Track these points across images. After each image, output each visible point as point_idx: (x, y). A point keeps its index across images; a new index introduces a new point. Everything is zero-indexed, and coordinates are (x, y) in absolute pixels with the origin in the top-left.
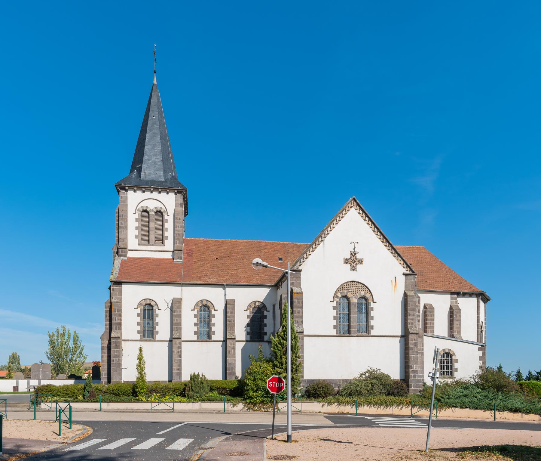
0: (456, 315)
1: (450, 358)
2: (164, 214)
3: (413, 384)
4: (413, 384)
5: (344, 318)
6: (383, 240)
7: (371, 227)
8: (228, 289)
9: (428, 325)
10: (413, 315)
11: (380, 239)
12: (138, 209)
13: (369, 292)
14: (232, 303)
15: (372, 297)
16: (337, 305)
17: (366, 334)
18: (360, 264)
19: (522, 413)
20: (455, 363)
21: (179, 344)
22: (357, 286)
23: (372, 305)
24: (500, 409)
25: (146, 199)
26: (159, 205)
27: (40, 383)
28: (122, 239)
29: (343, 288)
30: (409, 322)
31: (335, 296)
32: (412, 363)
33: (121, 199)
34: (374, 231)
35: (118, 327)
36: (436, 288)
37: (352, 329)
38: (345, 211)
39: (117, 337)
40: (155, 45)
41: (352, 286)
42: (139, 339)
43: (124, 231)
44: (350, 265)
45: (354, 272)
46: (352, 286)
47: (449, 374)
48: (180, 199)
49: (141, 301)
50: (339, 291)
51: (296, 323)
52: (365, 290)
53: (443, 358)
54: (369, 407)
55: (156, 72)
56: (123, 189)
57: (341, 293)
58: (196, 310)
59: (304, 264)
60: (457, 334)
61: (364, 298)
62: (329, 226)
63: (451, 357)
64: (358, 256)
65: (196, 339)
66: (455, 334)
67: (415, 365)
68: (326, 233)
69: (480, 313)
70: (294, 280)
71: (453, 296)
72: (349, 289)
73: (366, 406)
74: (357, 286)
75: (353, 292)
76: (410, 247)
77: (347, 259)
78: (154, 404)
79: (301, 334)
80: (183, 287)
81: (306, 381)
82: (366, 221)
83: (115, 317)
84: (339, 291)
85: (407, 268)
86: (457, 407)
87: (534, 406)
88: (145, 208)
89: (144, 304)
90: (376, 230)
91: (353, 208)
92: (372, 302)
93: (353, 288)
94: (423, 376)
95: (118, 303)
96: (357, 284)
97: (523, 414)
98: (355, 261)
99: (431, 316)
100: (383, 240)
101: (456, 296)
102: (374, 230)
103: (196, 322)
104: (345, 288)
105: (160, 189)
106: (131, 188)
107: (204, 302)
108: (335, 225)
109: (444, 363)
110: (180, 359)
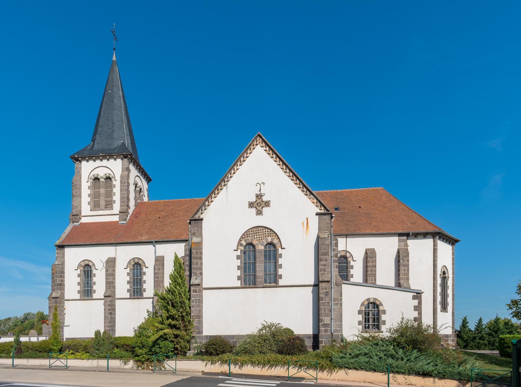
0: (403, 260)
1: (376, 309)
2: (112, 180)
3: (323, 340)
4: (323, 340)
5: (250, 268)
6: (293, 178)
7: (272, 157)
8: (158, 246)
9: (369, 273)
10: (326, 260)
11: (289, 176)
12: (90, 178)
13: (276, 237)
14: (160, 259)
15: (281, 243)
16: (241, 253)
17: (274, 284)
18: (267, 207)
19: (435, 377)
20: (382, 315)
21: (110, 302)
22: (263, 232)
23: (280, 251)
24: (404, 372)
25: (97, 168)
26: (108, 171)
27: (30, 339)
28: (76, 207)
29: (247, 235)
30: (321, 268)
31: (239, 244)
32: (322, 316)
33: (76, 170)
34: (282, 169)
35: (59, 288)
36: (380, 229)
37: (258, 279)
38: (250, 150)
39: (56, 297)
40: (114, 24)
41: (257, 231)
42: (79, 298)
43: (77, 199)
44: (255, 209)
45: (260, 216)
46: (257, 231)
47: (375, 327)
48: (126, 164)
49: (80, 262)
50: (243, 238)
51: (194, 276)
52: (272, 235)
53: (367, 310)
54: (252, 367)
55: (116, 49)
56: (77, 160)
57: (245, 240)
58: (129, 268)
59: (205, 211)
60: (404, 281)
61: (271, 244)
62: (232, 168)
63: (378, 307)
64: (265, 199)
65: (128, 297)
66: (402, 282)
67: (326, 318)
68: (229, 176)
69: (437, 255)
70: (195, 230)
71: (401, 238)
72: (254, 236)
73: (249, 366)
74: (263, 232)
75: (259, 239)
76: (366, 189)
77: (253, 203)
78: (52, 361)
79: (197, 286)
80: (117, 247)
81: (208, 337)
82: (273, 159)
83: (56, 278)
84: (243, 238)
85: (321, 207)
86: (350, 369)
87: (450, 369)
88: (96, 176)
89: (84, 265)
90: (284, 167)
91: (258, 145)
92: (280, 249)
93: (259, 234)
94: (342, 330)
95: (59, 266)
96: (263, 229)
97: (435, 379)
98: (261, 204)
99: (372, 262)
100: (293, 178)
101: (405, 238)
102: (282, 167)
103: (129, 280)
104: (249, 234)
105: (108, 156)
106: (84, 158)
107: (136, 260)
108: (238, 167)
109: (369, 315)
110: (110, 317)
